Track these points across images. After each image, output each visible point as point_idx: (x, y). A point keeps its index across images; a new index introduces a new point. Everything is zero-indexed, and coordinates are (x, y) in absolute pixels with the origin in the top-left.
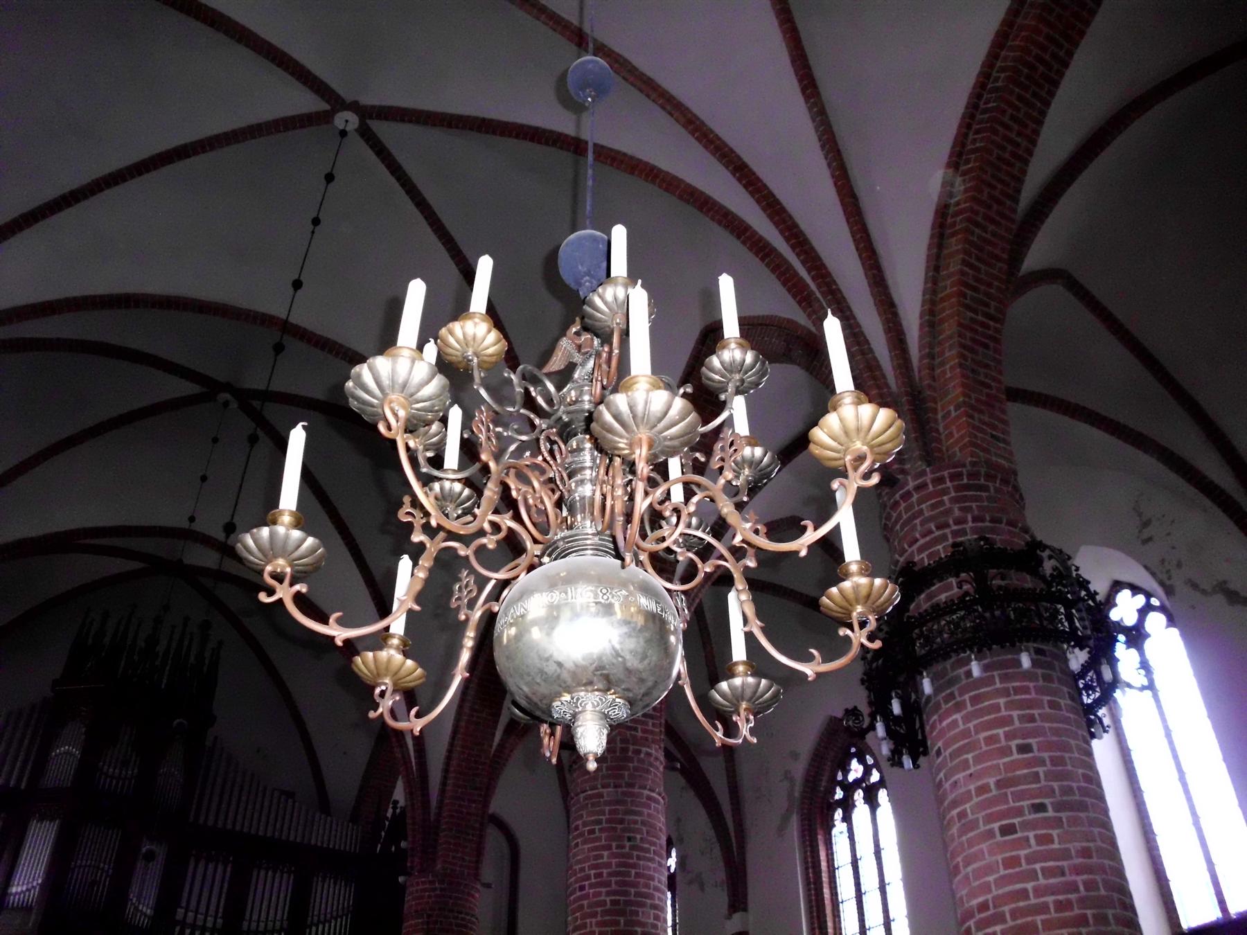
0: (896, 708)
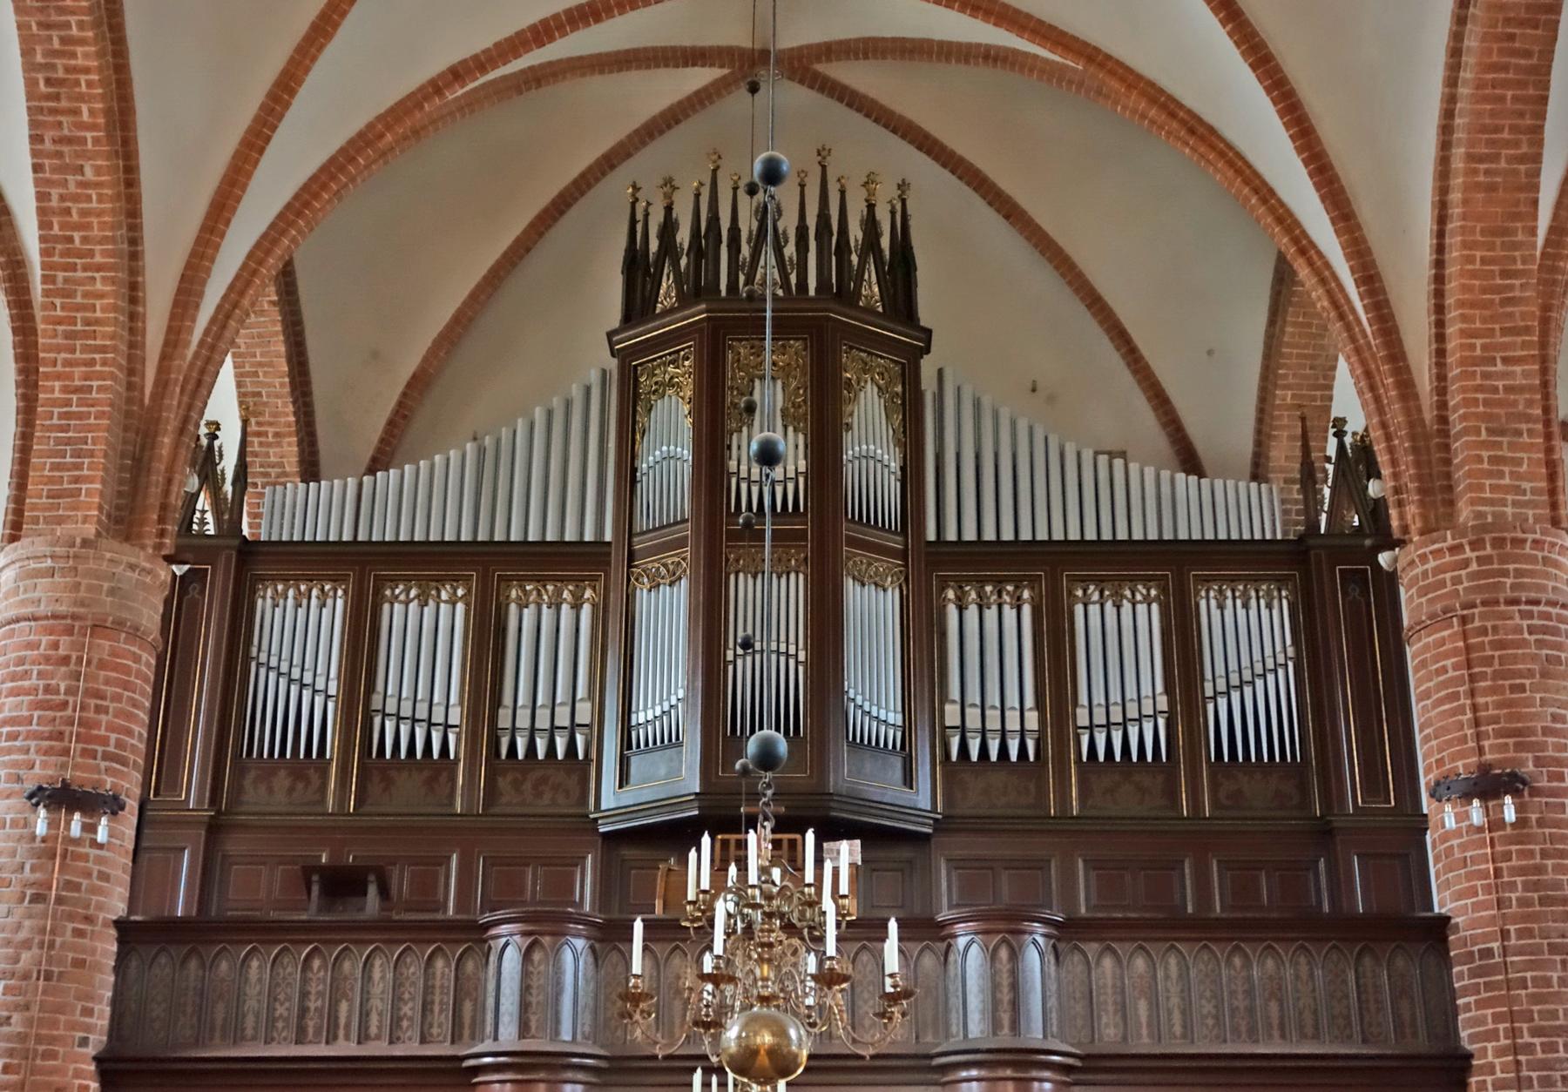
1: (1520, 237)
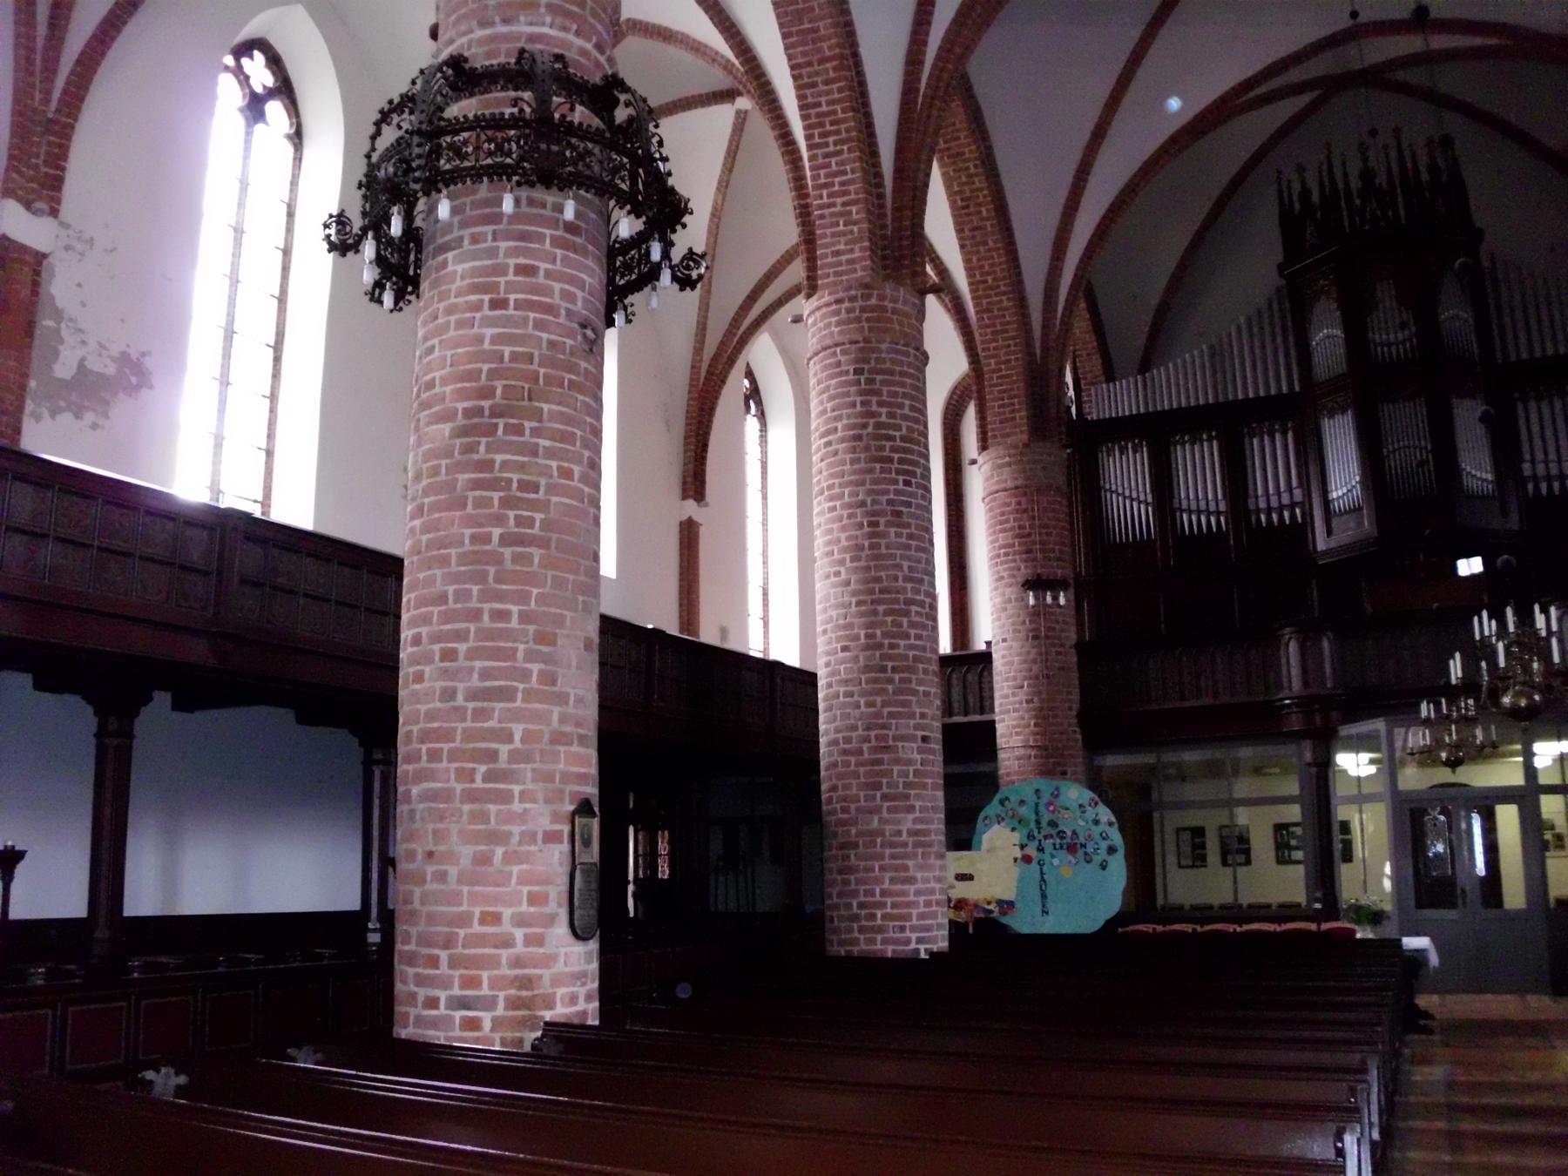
0: (396, 228)
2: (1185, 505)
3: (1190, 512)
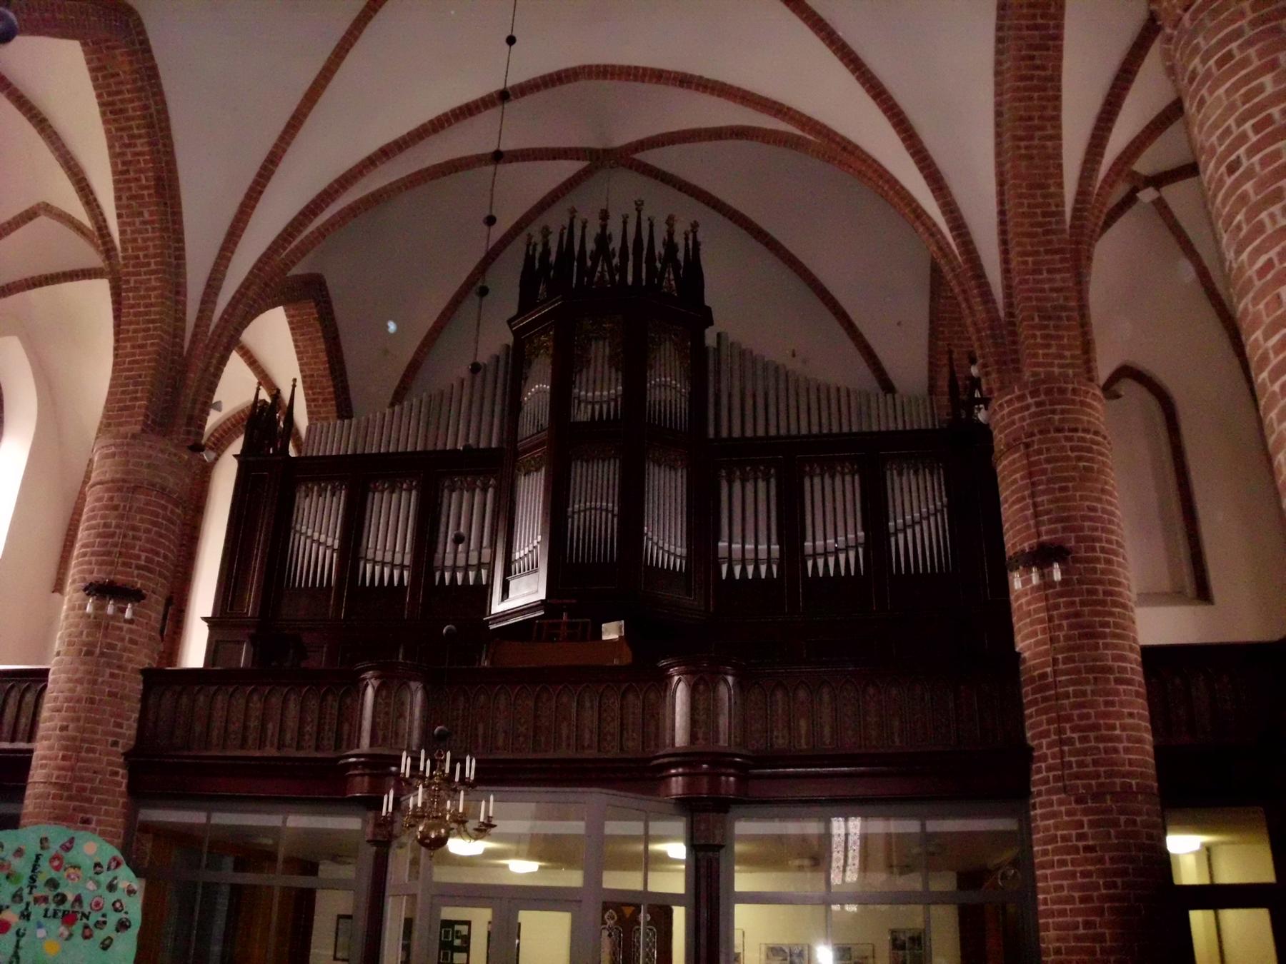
1: (1052, 189)
2: (370, 555)
3: (375, 562)
